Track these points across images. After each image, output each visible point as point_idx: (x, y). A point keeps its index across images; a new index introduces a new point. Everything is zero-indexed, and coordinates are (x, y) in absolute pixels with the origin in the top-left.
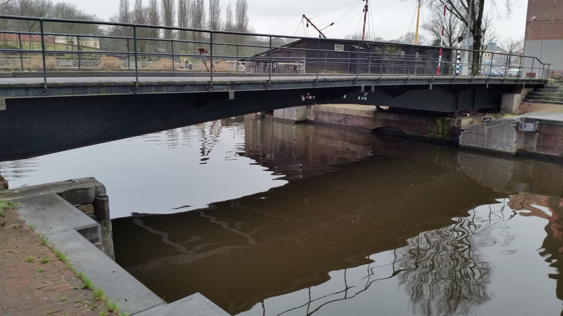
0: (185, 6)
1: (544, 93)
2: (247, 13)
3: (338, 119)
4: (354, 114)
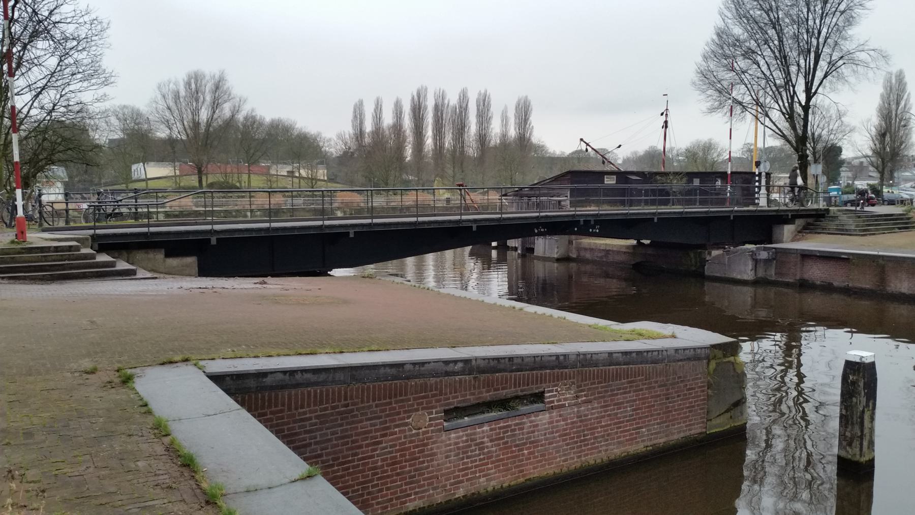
0: (442, 115)
1: (824, 223)
2: (530, 118)
3: (600, 255)
4: (615, 249)
